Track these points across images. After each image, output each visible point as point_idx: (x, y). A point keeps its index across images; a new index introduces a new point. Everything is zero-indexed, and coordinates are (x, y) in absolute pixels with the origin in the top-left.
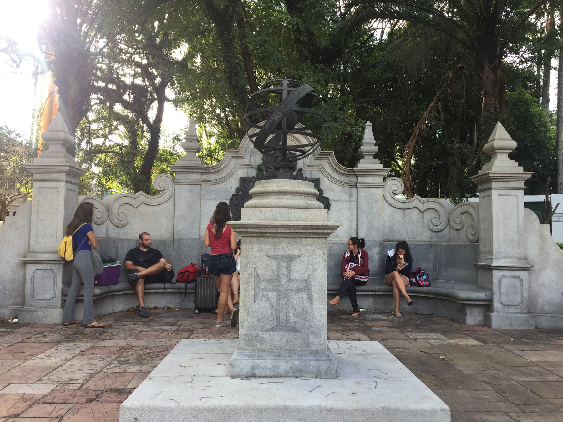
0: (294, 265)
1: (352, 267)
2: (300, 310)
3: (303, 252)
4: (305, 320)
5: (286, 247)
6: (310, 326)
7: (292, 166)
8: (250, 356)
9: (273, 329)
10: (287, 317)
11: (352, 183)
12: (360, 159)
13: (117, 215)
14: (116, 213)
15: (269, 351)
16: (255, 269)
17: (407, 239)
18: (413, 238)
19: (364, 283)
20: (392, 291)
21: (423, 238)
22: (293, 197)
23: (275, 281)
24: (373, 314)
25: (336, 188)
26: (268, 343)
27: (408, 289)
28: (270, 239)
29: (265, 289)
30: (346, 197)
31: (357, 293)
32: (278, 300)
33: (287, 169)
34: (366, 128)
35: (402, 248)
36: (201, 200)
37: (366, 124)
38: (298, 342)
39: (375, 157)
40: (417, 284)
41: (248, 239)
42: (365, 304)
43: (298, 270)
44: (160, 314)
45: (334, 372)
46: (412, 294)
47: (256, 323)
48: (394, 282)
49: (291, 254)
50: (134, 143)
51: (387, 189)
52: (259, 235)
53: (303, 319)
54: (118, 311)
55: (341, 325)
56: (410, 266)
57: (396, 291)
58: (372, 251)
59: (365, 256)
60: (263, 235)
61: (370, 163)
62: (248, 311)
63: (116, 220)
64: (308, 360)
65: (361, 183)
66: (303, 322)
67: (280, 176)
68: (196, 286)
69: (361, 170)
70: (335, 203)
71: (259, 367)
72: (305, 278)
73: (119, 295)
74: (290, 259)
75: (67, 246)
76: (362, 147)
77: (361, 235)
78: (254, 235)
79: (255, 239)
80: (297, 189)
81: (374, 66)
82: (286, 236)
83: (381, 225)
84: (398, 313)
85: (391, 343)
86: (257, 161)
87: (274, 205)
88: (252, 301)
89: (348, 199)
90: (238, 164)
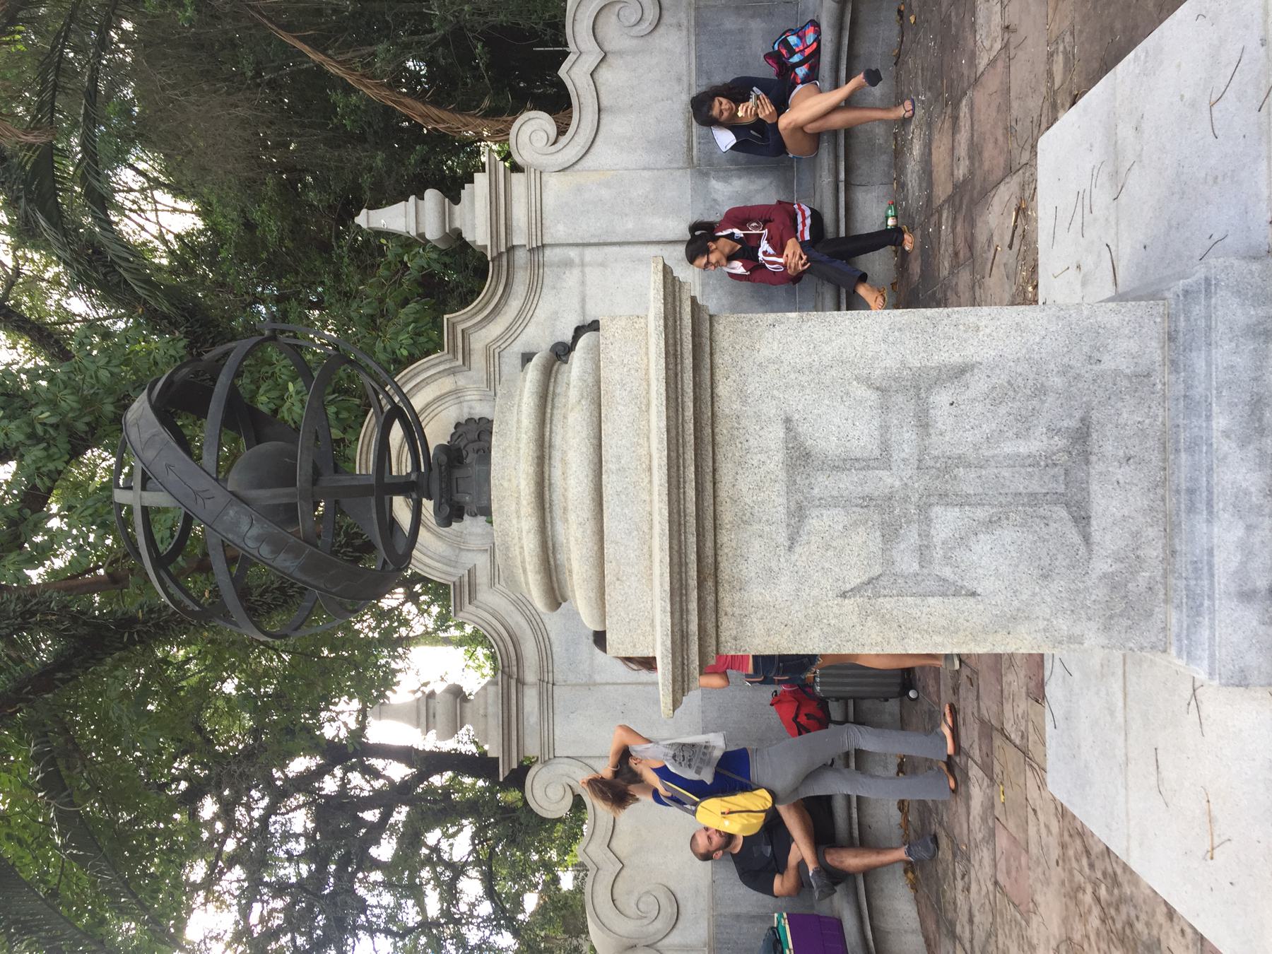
1: (771, 251)
2: (1003, 410)
3: (769, 409)
5: (753, 477)
6: (1064, 371)
8: (1196, 611)
9: (1082, 520)
10: (1031, 462)
13: (646, 922)
14: (639, 922)
15: (1171, 528)
16: (844, 595)
17: (685, 98)
18: (679, 80)
19: (817, 217)
20: (834, 133)
22: (557, 455)
23: (888, 516)
24: (902, 186)
25: (546, 306)
26: (1136, 535)
27: (827, 85)
28: (724, 538)
29: (923, 552)
30: (571, 278)
31: (842, 234)
32: (964, 501)
33: (458, 473)
34: (373, 225)
35: (711, 108)
36: (595, 684)
37: (364, 226)
38: (1130, 415)
39: (456, 200)
40: (813, 59)
42: (874, 212)
43: (843, 425)
45: (1255, 267)
46: (843, 74)
47: (1058, 585)
48: (810, 128)
49: (779, 457)
50: (472, 808)
52: (710, 583)
53: (1035, 402)
54: (915, 914)
55: (951, 273)
56: (765, 85)
57: (838, 120)
58: (719, 198)
59: (739, 217)
60: (709, 570)
62: (1010, 621)
63: (658, 925)
64: (1209, 375)
65: (530, 235)
66: (1051, 399)
67: (484, 503)
68: (837, 699)
70: (588, 306)
72: (873, 396)
73: (870, 914)
74: (800, 457)
76: (428, 236)
77: (680, 229)
79: (726, 599)
81: (249, 226)
82: (709, 478)
83: (646, 174)
84: (901, 112)
85: (1028, 105)
86: (479, 530)
87: (590, 527)
88: (972, 600)
89: (576, 272)
90: (492, 584)
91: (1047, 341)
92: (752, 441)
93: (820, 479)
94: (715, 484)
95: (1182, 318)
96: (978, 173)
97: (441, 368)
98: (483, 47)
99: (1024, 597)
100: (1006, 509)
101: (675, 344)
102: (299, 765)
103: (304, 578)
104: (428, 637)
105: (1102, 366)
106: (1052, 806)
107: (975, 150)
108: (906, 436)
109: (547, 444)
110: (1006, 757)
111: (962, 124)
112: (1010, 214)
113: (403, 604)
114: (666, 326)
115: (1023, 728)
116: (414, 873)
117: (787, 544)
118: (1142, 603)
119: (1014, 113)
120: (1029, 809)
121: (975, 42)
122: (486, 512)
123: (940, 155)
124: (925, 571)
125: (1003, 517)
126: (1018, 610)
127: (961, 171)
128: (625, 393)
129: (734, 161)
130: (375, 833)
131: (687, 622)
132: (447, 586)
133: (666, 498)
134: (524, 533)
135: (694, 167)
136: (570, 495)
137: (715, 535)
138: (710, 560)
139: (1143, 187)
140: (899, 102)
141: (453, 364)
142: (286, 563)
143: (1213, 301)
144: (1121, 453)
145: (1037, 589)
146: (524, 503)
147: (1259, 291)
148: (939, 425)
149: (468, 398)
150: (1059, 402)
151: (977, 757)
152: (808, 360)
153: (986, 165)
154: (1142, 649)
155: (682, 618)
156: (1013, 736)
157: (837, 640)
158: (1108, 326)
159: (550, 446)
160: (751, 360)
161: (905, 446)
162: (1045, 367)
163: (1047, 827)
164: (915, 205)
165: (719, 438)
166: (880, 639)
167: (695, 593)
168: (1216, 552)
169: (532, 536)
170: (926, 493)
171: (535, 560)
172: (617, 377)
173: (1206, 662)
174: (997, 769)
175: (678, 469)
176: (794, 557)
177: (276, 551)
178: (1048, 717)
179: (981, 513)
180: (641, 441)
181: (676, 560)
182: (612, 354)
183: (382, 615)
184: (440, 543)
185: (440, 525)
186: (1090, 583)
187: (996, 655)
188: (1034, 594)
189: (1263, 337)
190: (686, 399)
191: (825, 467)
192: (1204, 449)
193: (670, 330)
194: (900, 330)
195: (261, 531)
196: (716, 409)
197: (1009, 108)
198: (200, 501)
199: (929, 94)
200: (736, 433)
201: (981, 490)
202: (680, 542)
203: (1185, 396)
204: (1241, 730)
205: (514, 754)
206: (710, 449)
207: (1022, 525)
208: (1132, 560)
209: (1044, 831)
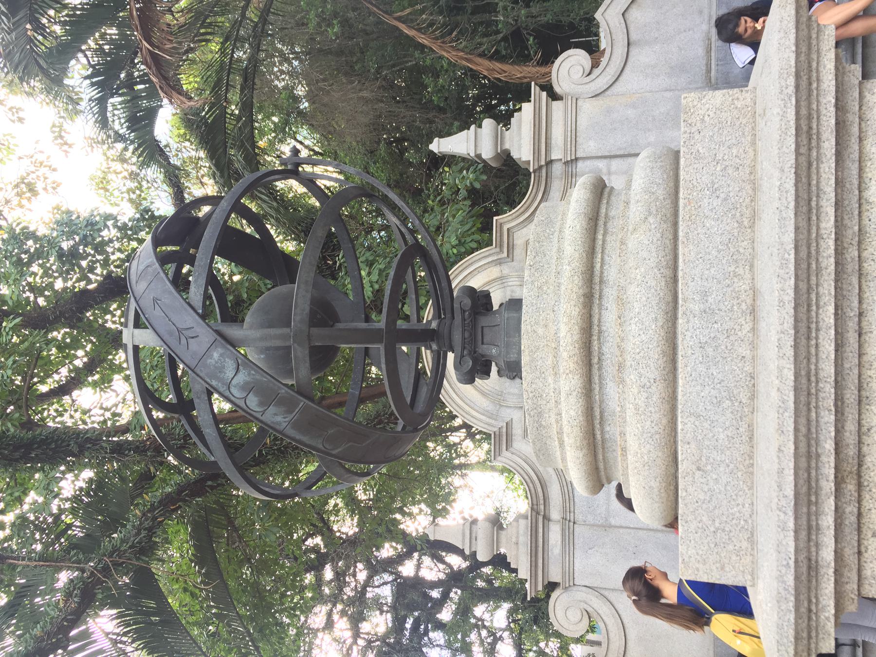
7: (467, 302)
11: (566, 173)
12: (512, 158)
22: (610, 294)
35: (737, 25)
36: (611, 526)
37: (436, 151)
51: (579, 89)
60: (850, 466)
61: (520, 134)
65: (565, 150)
67: (513, 357)
69: (536, 151)
76: (484, 156)
82: (852, 325)
83: (668, 94)
87: (658, 391)
97: (490, 259)
98: (534, 39)
101: (809, 118)
102: (387, 551)
103: (298, 437)
104: (483, 465)
109: (597, 279)
113: (463, 441)
114: (797, 87)
116: (465, 635)
122: (513, 370)
128: (716, 202)
130: (439, 604)
131: (817, 545)
132: (490, 435)
133: (790, 352)
136: (629, 346)
138: (852, 451)
141: (500, 257)
142: (276, 417)
146: (565, 355)
149: (510, 284)
155: (809, 540)
167: (832, 501)
169: (573, 400)
172: (706, 179)
175: (809, 311)
177: (265, 403)
180: (740, 271)
181: (803, 449)
183: (450, 447)
184: (484, 400)
185: (460, 381)
190: (823, 203)
195: (247, 379)
196: (865, 221)
198: (184, 341)
202: (809, 421)
206: (855, 281)
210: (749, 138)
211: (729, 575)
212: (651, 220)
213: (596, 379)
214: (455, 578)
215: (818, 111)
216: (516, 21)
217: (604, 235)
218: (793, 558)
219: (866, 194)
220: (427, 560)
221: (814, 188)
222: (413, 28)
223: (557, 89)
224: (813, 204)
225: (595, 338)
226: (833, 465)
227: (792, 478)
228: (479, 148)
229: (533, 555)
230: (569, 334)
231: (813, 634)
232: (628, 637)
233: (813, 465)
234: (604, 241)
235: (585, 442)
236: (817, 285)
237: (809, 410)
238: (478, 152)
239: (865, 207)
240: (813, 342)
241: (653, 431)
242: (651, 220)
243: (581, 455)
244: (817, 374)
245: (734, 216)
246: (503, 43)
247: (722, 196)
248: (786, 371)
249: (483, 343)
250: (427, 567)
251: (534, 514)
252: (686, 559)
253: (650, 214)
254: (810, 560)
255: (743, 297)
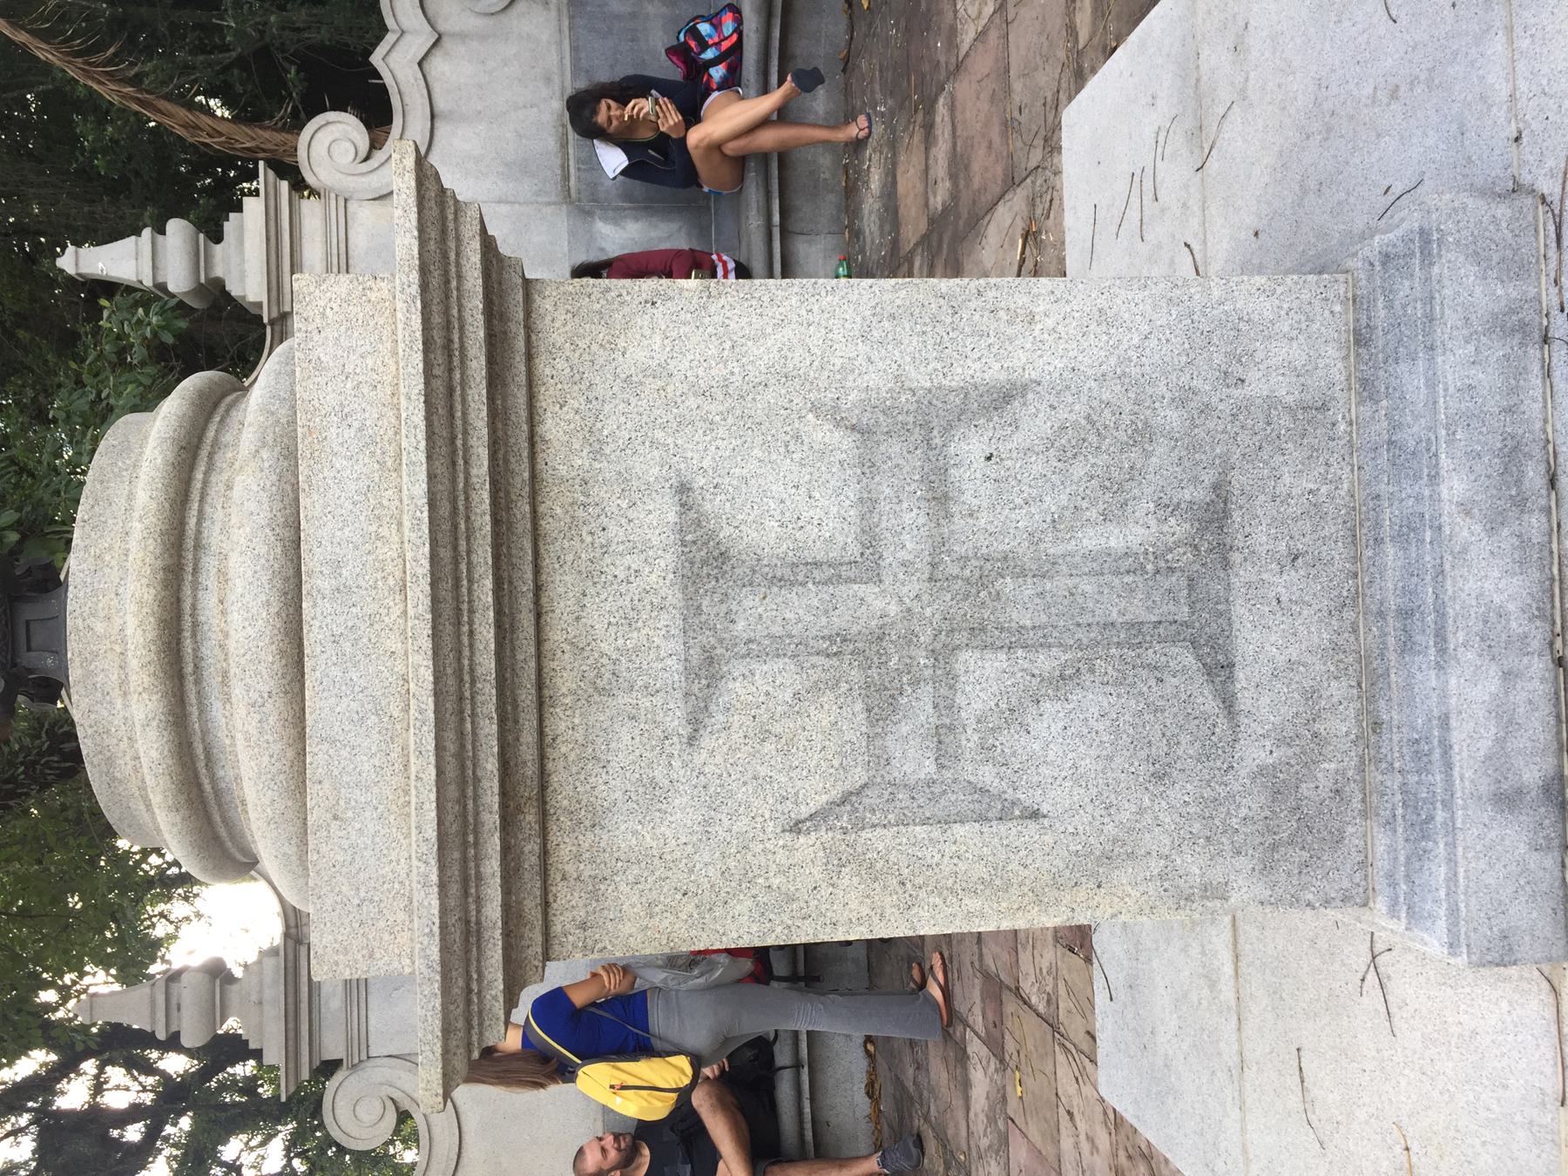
0: (751, 535)
2: (1079, 470)
3: (647, 466)
4: (1143, 435)
5: (615, 601)
8: (1421, 829)
9: (1220, 670)
10: (1130, 565)
15: (1370, 682)
16: (796, 828)
17: (557, 105)
18: (548, 80)
20: (764, 157)
21: (545, 37)
22: (210, 563)
23: (877, 671)
24: (857, 234)
26: (1311, 695)
28: (560, 723)
32: (1015, 640)
34: (84, 270)
35: (595, 112)
37: (71, 270)
38: (1296, 480)
39: (217, 237)
41: (569, 904)
43: (788, 499)
44: (898, 1082)
45: (1503, 211)
46: (774, 78)
47: (1182, 791)
48: (731, 148)
49: (668, 560)
51: (350, 183)
52: (530, 817)
53: (1134, 454)
57: (768, 138)
60: (528, 790)
66: (1161, 448)
71: (1498, 760)
72: (844, 442)
74: (707, 562)
75: (631, 1081)
76: (171, 288)
78: (531, 861)
79: (565, 847)
80: (137, 527)
82: (526, 602)
84: (853, 131)
87: (275, 710)
91: (1153, 343)
92: (613, 529)
93: (748, 603)
94: (538, 616)
95: (1380, 304)
96: (965, 198)
98: (298, 72)
99: (1125, 816)
100: (1089, 653)
105: (1247, 391)
106: (1099, 1109)
107: (959, 165)
108: (908, 518)
109: (190, 543)
110: (1024, 1031)
111: (938, 132)
112: (1013, 244)
114: (424, 287)
115: (1049, 989)
117: (685, 731)
118: (1318, 824)
119: (1017, 98)
120: (1062, 1111)
121: (955, 12)
123: (908, 181)
124: (948, 774)
125: (1084, 668)
126: (1115, 841)
127: (939, 200)
129: (628, 197)
134: (138, 728)
135: (571, 203)
136: (231, 645)
137: (541, 719)
138: (530, 770)
139: (1248, 143)
140: (849, 117)
143: (1436, 270)
144: (1282, 546)
145: (1147, 803)
146: (134, 663)
147: (1509, 253)
148: (967, 497)
150: (1175, 454)
151: (980, 1027)
152: (719, 371)
153: (976, 182)
154: (1327, 903)
155: (466, 894)
156: (1034, 1000)
157: (785, 917)
158: (1255, 317)
159: (198, 546)
160: (610, 368)
161: (906, 537)
162: (1150, 391)
163: (1091, 1139)
164: (875, 257)
165: (546, 525)
166: (865, 911)
168: (1453, 723)
169: (152, 733)
170: (946, 626)
171: (165, 782)
172: (332, 399)
173: (1442, 924)
174: (1010, 1046)
175: (457, 586)
176: (700, 758)
178: (1099, 983)
179: (1046, 662)
180: (384, 531)
181: (451, 771)
182: (319, 352)
186: (1236, 787)
187: (1079, 927)
188: (1141, 811)
189: (1518, 336)
190: (473, 442)
191: (758, 578)
192: (1428, 535)
193: (436, 295)
194: (892, 316)
196: (541, 466)
197: (1008, 91)
199: (890, 102)
200: (580, 513)
201: (1044, 618)
202: (461, 735)
203: (1390, 442)
204: (1475, 1033)
205: (305, 1059)
207: (1118, 683)
208: (1306, 741)
209: (1085, 1147)
210: (389, 345)
211: (380, 963)
212: (265, 454)
213: (192, 697)
214: (174, 1096)
215: (461, 318)
216: (262, 33)
217: (207, 473)
218: (437, 921)
219: (540, 430)
220: (116, 1074)
221: (459, 422)
222: (23, 28)
223: (310, 179)
224: (459, 443)
225: (187, 634)
226: (496, 790)
227: (434, 814)
228: (161, 272)
229: (291, 1018)
230: (139, 631)
231: (475, 1022)
232: (464, 1128)
233: (470, 793)
234: (205, 483)
235: (182, 799)
236: (469, 552)
237: (462, 720)
238: (160, 280)
239: (540, 446)
240: (465, 628)
241: (274, 770)
242: (265, 454)
243: (178, 819)
244: (472, 670)
245: (373, 454)
246: (236, 72)
247: (356, 424)
248: (422, 669)
249: (29, 649)
250: (117, 1088)
251: (291, 943)
252: (320, 952)
253: (264, 445)
254: (468, 922)
255: (390, 568)
